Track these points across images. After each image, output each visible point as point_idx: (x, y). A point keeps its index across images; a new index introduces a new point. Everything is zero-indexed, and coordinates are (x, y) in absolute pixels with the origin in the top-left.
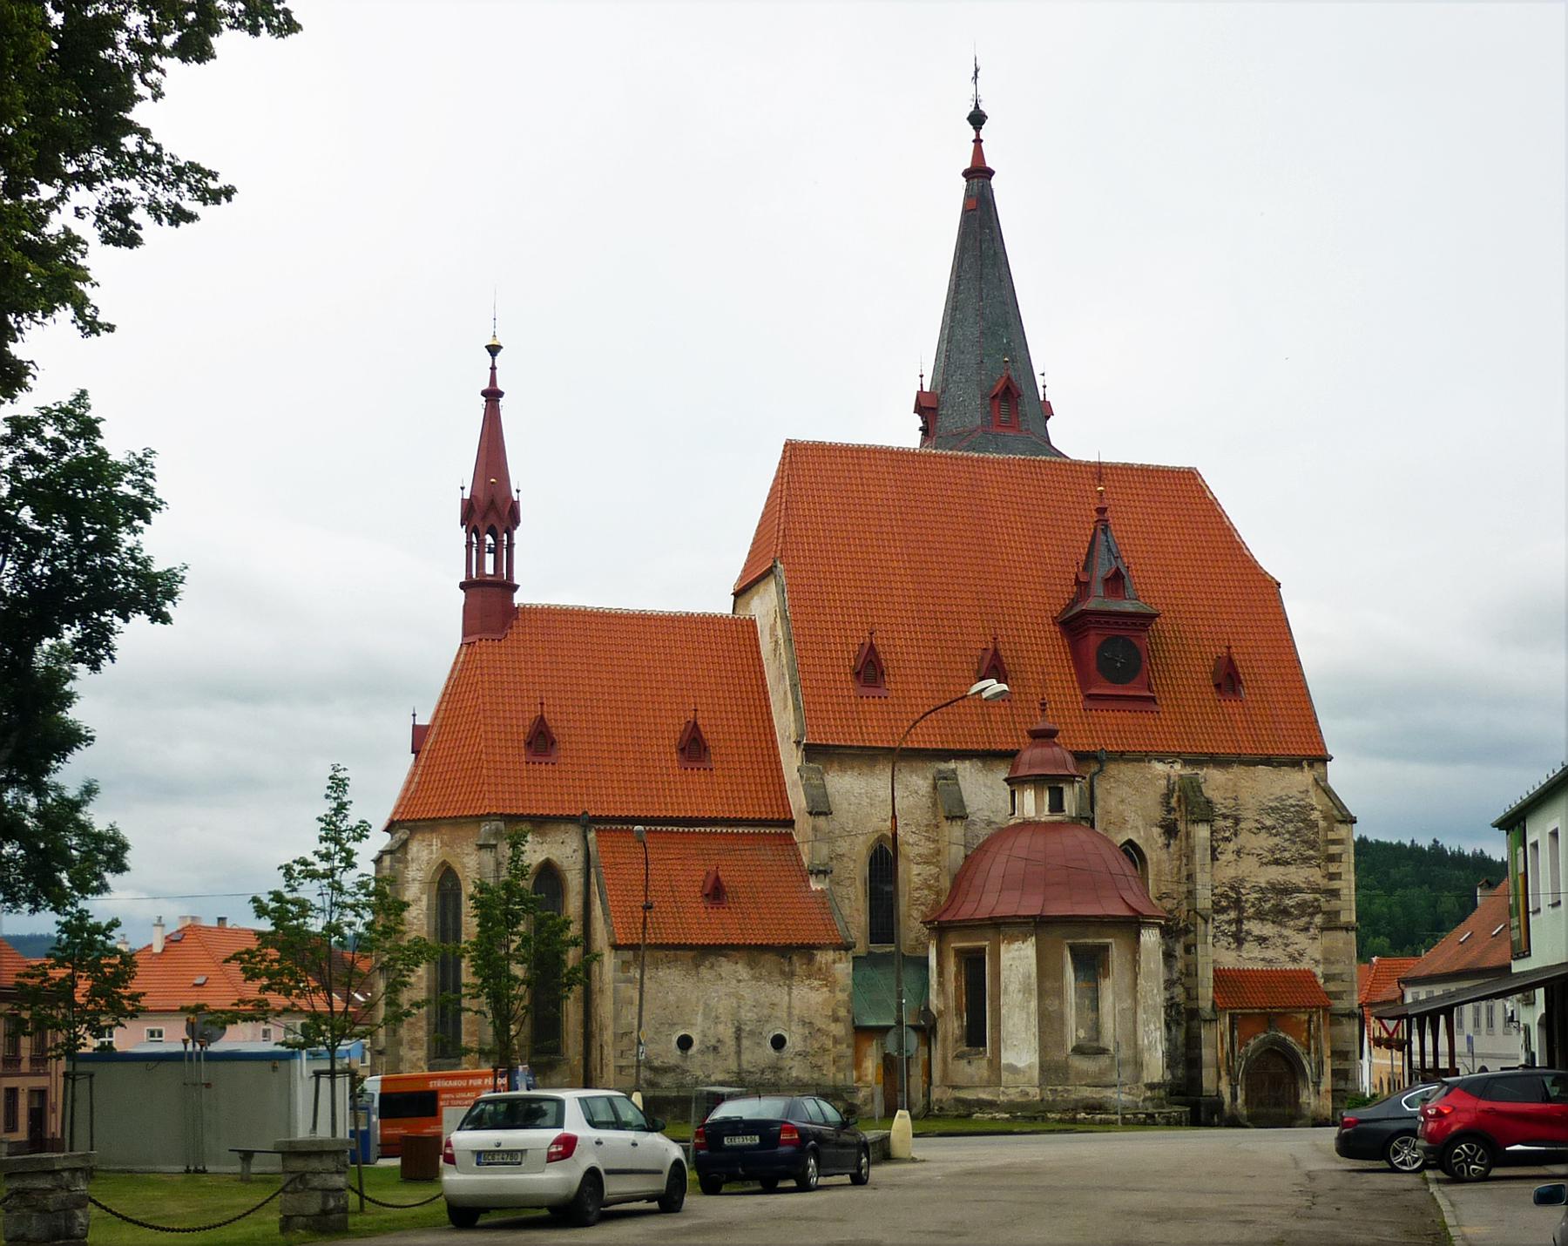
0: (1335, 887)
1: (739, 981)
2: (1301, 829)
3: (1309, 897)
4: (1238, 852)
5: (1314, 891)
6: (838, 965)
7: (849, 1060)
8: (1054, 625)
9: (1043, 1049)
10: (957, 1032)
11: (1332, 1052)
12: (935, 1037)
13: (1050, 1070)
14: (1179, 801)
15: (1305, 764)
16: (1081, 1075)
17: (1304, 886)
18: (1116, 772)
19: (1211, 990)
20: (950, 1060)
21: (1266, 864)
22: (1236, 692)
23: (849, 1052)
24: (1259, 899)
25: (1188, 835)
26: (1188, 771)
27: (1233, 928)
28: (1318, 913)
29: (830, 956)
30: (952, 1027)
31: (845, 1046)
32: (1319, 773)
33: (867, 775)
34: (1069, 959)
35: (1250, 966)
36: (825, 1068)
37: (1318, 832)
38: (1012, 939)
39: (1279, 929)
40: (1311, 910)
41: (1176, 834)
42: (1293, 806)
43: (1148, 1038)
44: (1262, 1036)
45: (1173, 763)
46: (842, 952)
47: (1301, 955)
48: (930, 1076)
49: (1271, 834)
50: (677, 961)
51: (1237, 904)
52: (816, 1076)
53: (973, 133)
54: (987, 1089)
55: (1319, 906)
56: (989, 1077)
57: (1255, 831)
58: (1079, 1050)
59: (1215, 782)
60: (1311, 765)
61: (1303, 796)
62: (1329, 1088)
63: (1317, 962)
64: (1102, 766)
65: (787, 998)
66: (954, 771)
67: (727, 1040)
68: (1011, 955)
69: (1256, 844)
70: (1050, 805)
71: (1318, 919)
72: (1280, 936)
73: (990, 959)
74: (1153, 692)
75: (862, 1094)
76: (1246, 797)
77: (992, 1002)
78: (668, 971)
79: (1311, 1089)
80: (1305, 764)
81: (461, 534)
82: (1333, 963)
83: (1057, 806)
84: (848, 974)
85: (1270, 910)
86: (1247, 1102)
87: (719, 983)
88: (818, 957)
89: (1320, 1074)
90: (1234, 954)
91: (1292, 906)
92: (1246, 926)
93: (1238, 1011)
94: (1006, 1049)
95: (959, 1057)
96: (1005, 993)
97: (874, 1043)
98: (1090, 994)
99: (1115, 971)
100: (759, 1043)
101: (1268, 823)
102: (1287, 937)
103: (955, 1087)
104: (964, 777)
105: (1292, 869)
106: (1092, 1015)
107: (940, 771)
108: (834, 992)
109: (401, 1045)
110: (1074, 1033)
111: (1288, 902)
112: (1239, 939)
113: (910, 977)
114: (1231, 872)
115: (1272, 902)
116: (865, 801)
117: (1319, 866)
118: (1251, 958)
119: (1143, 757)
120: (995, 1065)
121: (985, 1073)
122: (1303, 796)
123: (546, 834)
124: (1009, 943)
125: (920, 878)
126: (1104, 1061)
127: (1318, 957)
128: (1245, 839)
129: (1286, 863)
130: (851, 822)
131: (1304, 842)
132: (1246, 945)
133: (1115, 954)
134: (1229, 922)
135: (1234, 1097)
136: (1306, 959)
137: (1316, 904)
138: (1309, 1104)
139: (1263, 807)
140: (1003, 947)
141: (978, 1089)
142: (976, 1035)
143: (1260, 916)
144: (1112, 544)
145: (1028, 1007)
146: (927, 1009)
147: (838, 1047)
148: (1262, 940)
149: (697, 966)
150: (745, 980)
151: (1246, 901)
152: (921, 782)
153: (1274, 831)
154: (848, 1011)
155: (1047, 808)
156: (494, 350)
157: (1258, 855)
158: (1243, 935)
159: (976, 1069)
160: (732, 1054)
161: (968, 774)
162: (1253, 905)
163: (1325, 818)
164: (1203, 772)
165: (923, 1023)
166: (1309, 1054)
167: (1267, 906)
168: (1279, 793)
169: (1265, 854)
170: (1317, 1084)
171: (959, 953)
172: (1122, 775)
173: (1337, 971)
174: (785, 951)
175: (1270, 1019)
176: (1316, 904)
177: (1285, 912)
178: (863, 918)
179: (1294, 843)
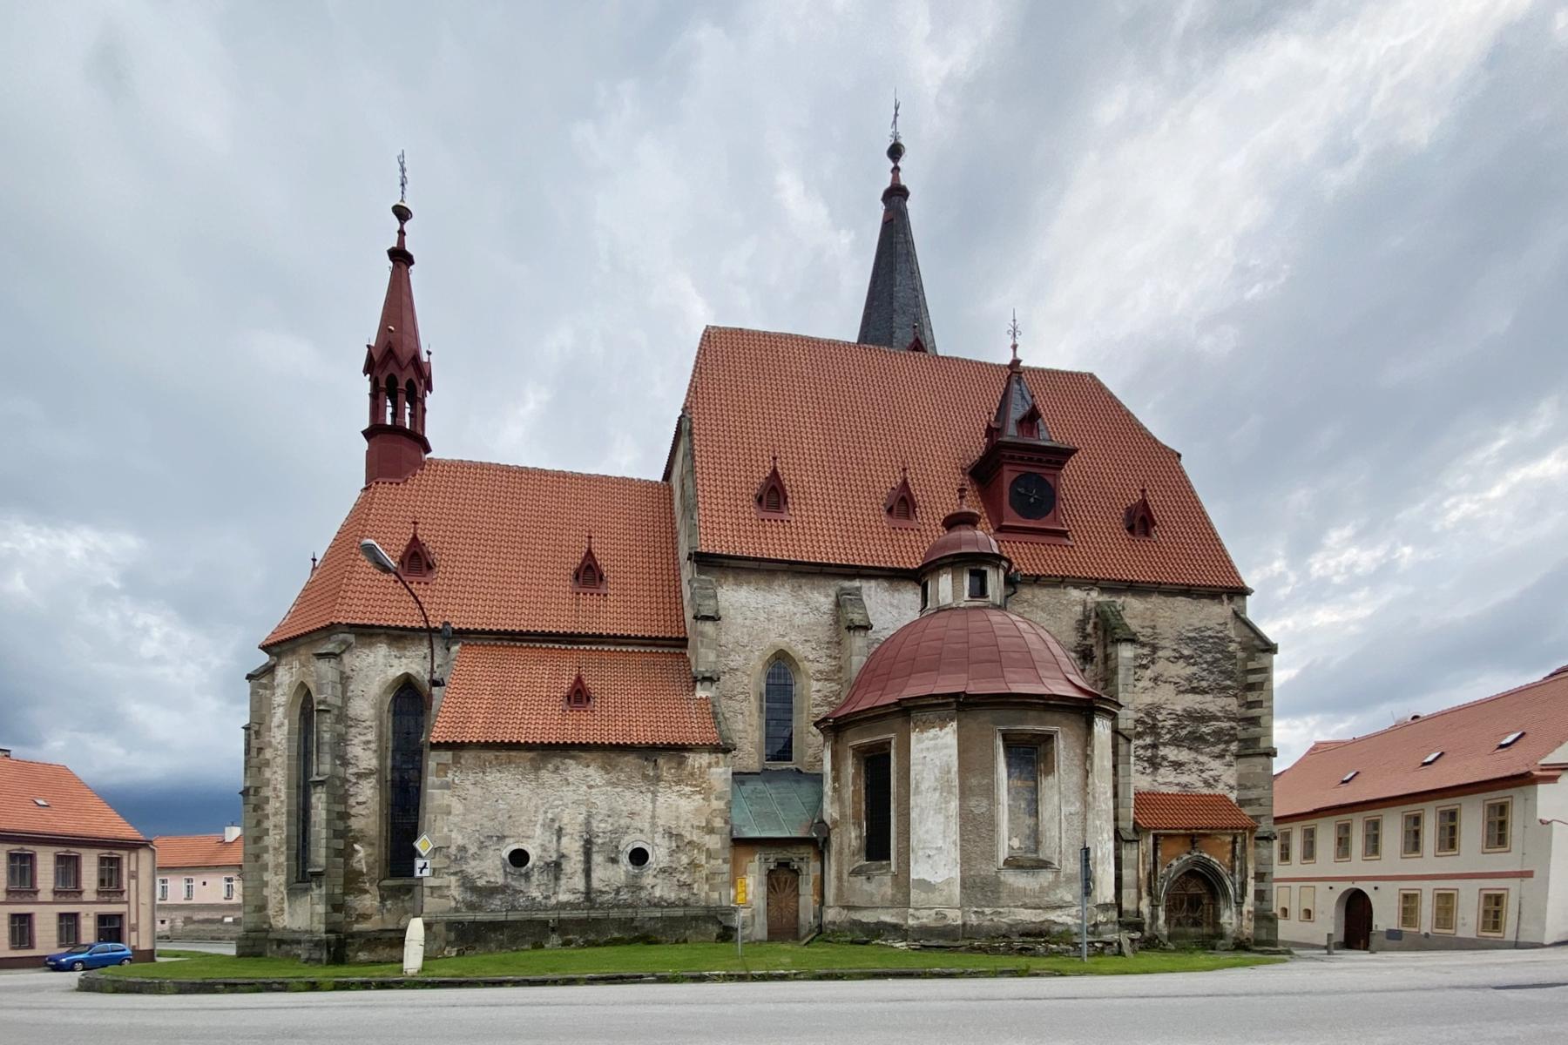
0: (1255, 715)
1: (590, 787)
2: (1220, 659)
3: (1225, 725)
4: (1155, 680)
5: (1230, 719)
6: (713, 770)
7: (726, 877)
8: (963, 474)
9: (966, 860)
10: (854, 843)
11: (1256, 873)
12: (829, 851)
13: (977, 887)
14: (1095, 626)
15: (1225, 597)
16: (1015, 893)
17: (1220, 714)
18: (1030, 597)
19: (1132, 810)
20: (845, 876)
21: (1183, 692)
22: (1147, 534)
23: (726, 867)
24: (1175, 726)
25: (1107, 658)
26: (1105, 598)
27: (1149, 753)
28: (1234, 741)
29: (705, 758)
30: (849, 837)
31: (720, 861)
32: (1239, 607)
33: (764, 590)
34: (1001, 750)
35: (1164, 789)
36: (696, 886)
37: (1235, 664)
38: (926, 726)
39: (1195, 755)
40: (1227, 738)
41: (1092, 660)
42: (1210, 637)
43: (1102, 849)
44: (1186, 857)
45: (1089, 590)
46: (720, 755)
47: (1216, 781)
48: (822, 895)
49: (1189, 664)
50: (510, 763)
51: (1153, 729)
52: (684, 895)
53: (892, 165)
54: (890, 910)
55: (1235, 734)
56: (893, 895)
57: (1172, 659)
58: (1013, 863)
59: (1134, 610)
60: (1230, 599)
61: (1222, 628)
62: (1252, 909)
63: (1232, 788)
64: (1015, 589)
65: (650, 806)
66: (859, 589)
67: (573, 855)
68: (923, 746)
69: (1173, 673)
70: (970, 590)
71: (1234, 747)
72: (1196, 762)
73: (897, 754)
74: (1063, 526)
75: (743, 914)
76: (1163, 626)
77: (898, 805)
78: (498, 775)
79: (1234, 909)
80: (1225, 597)
81: (365, 384)
82: (1249, 788)
83: (980, 590)
84: (726, 780)
85: (1186, 737)
86: (1167, 921)
87: (564, 789)
88: (690, 761)
89: (1243, 894)
90: (1149, 779)
91: (1208, 734)
92: (1163, 751)
93: (1162, 831)
94: (916, 862)
95: (856, 872)
96: (918, 792)
97: (757, 857)
98: (1028, 795)
99: (1062, 767)
100: (545, 850)
101: (1186, 652)
102: (1203, 764)
103: (850, 908)
104: (869, 596)
105: (1209, 697)
106: (1030, 821)
107: (842, 589)
108: (710, 801)
109: (267, 870)
110: (1007, 842)
111: (1204, 729)
112: (1154, 764)
113: (806, 788)
114: (1147, 699)
115: (1189, 729)
116: (762, 617)
117: (1235, 696)
118: (1166, 781)
119: (1062, 582)
120: (903, 881)
121: (888, 890)
122: (1222, 628)
123: (405, 648)
124: (922, 731)
125: (820, 694)
126: (1046, 877)
127: (1233, 782)
128: (1160, 667)
129: (1204, 692)
130: (746, 637)
131: (1221, 672)
132: (1162, 770)
133: (1061, 746)
134: (1145, 747)
135: (1154, 917)
136: (1221, 786)
137: (1232, 732)
138: (1231, 924)
139: (1182, 637)
140: (913, 736)
141: (879, 910)
142: (877, 846)
143: (1176, 742)
144: (1025, 393)
145: (946, 809)
146: (822, 821)
147: (712, 862)
148: (1177, 765)
149: (537, 769)
150: (598, 786)
151: (1163, 727)
152: (822, 599)
153: (1192, 661)
154: (726, 822)
155: (966, 594)
156: (402, 213)
157: (1175, 683)
158: (1158, 760)
159: (881, 886)
160: (580, 871)
161: (873, 593)
162: (1169, 732)
163: (1244, 649)
164: (1120, 600)
165: (815, 835)
166: (1233, 873)
167: (1184, 733)
168: (1198, 625)
169: (1183, 682)
170: (1240, 905)
171: (860, 752)
172: (1036, 600)
173: (1253, 797)
174: (650, 751)
175: (1193, 839)
176: (1232, 732)
177: (1201, 739)
178: (757, 734)
179: (1212, 673)
